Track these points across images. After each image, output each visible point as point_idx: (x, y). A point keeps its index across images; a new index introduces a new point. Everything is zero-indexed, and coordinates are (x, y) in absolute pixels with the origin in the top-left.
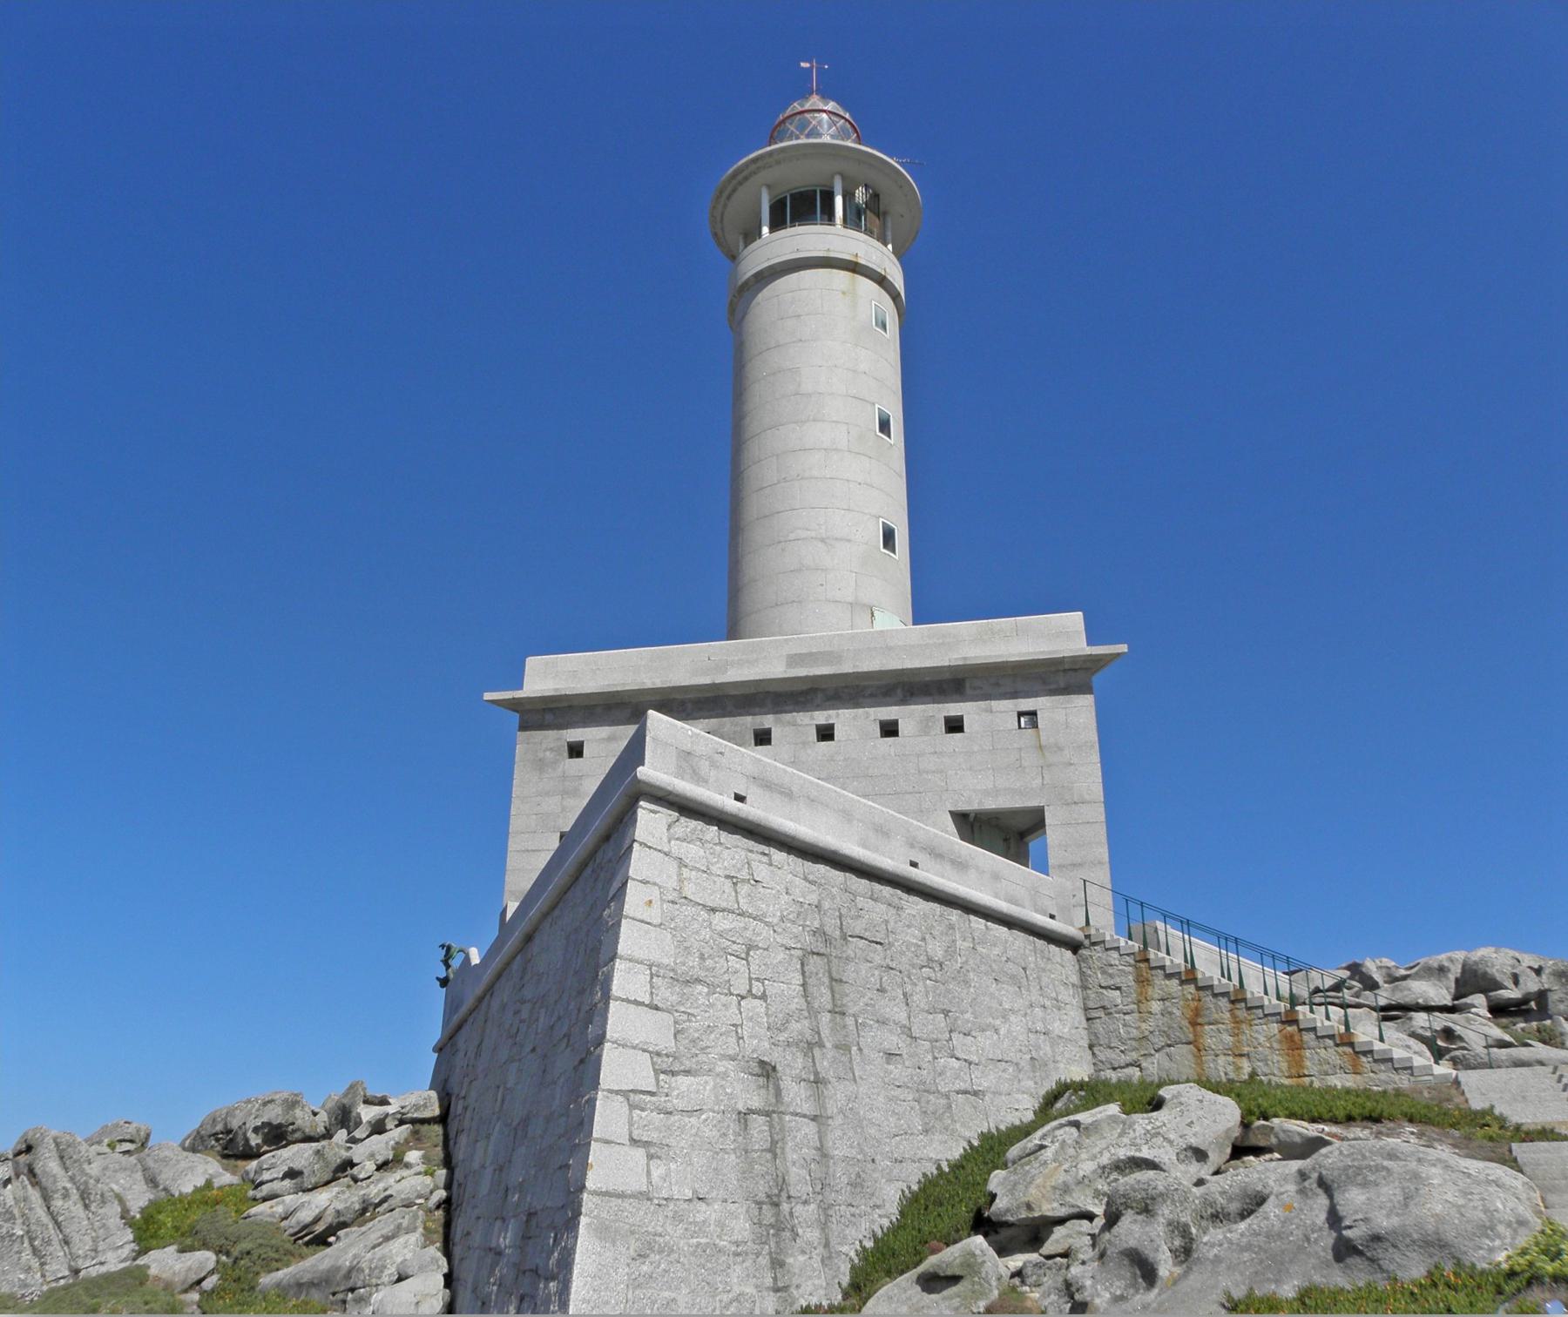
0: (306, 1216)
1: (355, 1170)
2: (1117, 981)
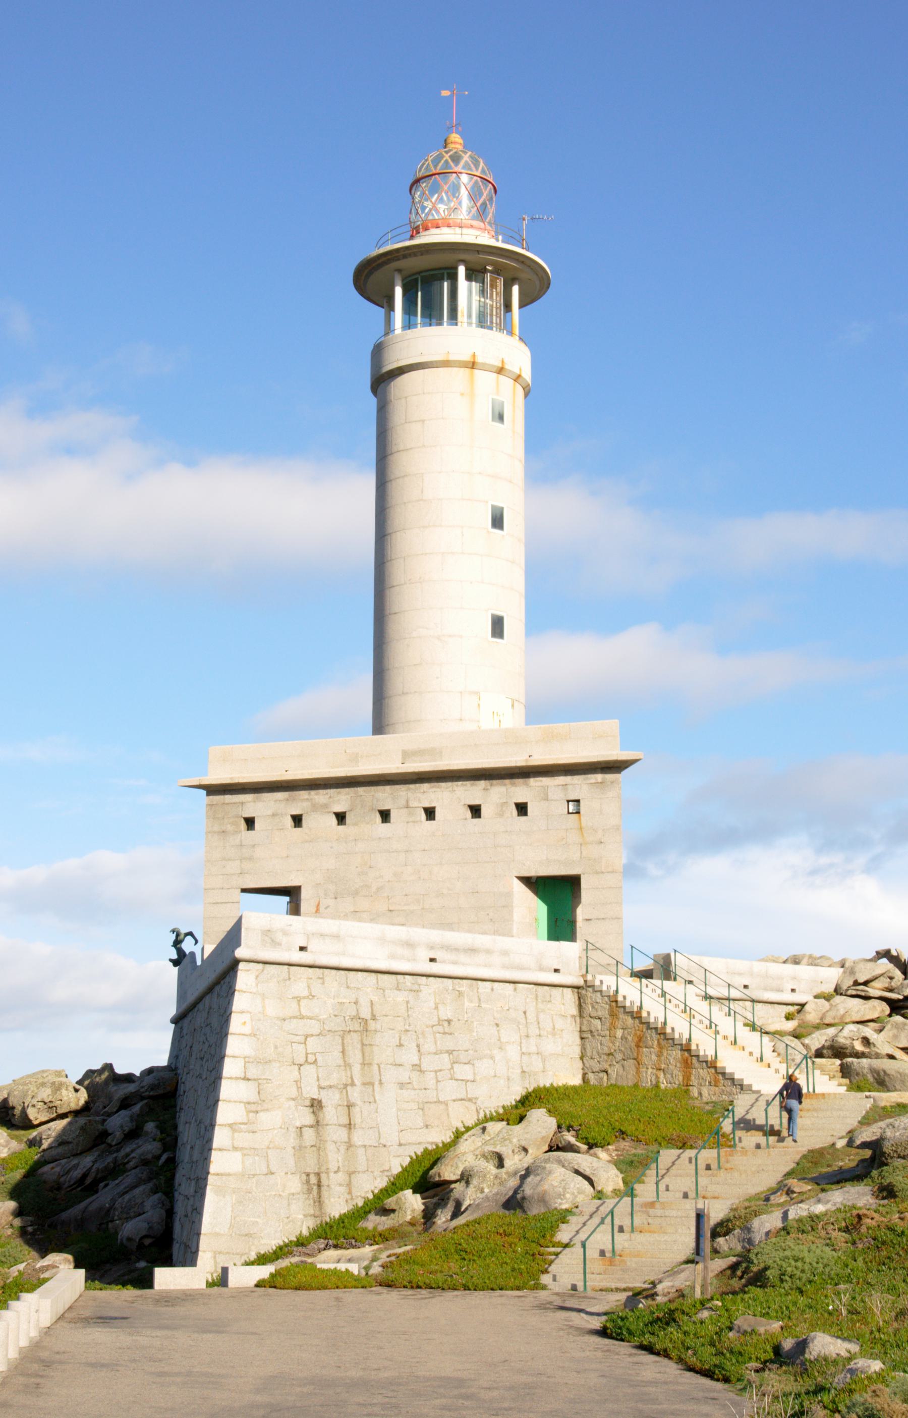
0: (77, 1174)
1: (109, 1140)
2: (600, 1014)
